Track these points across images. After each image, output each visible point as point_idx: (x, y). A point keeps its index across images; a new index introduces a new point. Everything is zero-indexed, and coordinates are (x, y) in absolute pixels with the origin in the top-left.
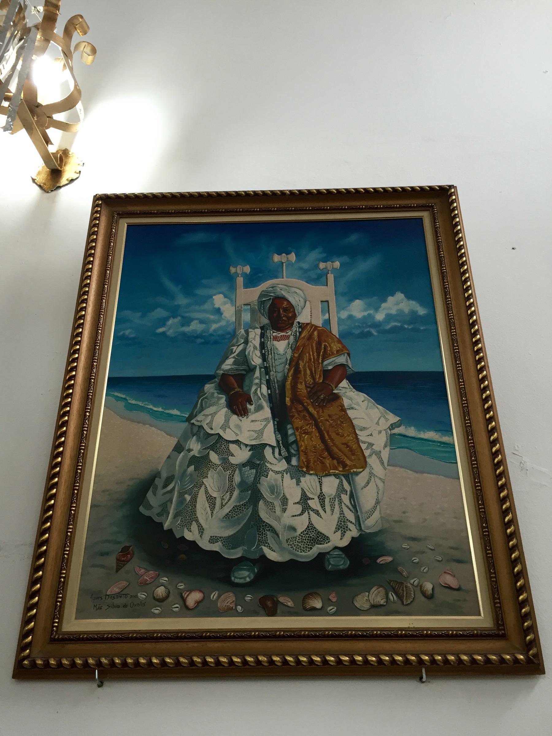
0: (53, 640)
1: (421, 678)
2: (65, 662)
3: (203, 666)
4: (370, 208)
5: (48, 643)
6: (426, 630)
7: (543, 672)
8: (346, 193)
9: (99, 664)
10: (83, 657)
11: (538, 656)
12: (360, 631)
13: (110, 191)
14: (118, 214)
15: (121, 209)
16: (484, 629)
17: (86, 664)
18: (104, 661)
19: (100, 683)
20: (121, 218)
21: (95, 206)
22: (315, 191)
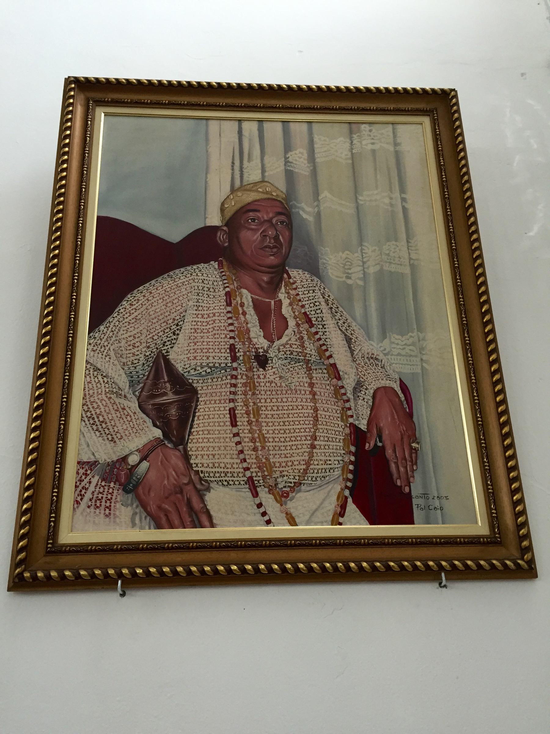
0: (49, 553)
1: (440, 584)
2: (53, 574)
3: (174, 576)
4: (136, 102)
5: (44, 556)
6: (339, 539)
7: (537, 577)
8: (106, 84)
9: (120, 575)
10: (172, 566)
11: (531, 562)
12: (200, 542)
13: (81, 73)
14: (94, 101)
15: (99, 96)
16: (483, 537)
17: (106, 575)
18: (125, 571)
19: (121, 593)
20: (97, 106)
21: (66, 91)
22: (114, 80)
